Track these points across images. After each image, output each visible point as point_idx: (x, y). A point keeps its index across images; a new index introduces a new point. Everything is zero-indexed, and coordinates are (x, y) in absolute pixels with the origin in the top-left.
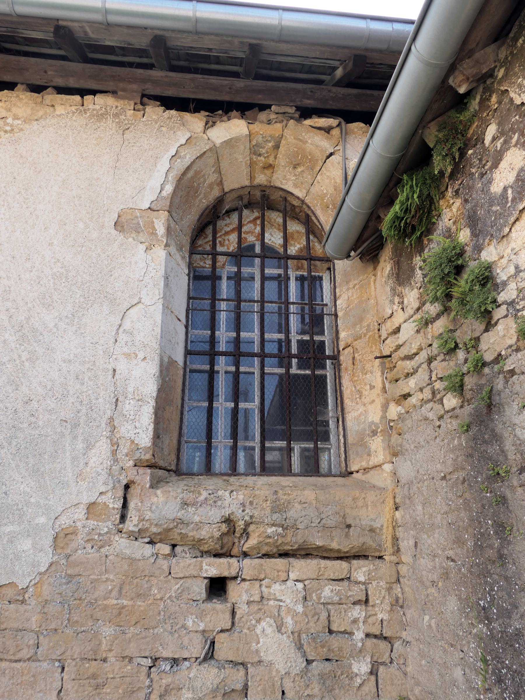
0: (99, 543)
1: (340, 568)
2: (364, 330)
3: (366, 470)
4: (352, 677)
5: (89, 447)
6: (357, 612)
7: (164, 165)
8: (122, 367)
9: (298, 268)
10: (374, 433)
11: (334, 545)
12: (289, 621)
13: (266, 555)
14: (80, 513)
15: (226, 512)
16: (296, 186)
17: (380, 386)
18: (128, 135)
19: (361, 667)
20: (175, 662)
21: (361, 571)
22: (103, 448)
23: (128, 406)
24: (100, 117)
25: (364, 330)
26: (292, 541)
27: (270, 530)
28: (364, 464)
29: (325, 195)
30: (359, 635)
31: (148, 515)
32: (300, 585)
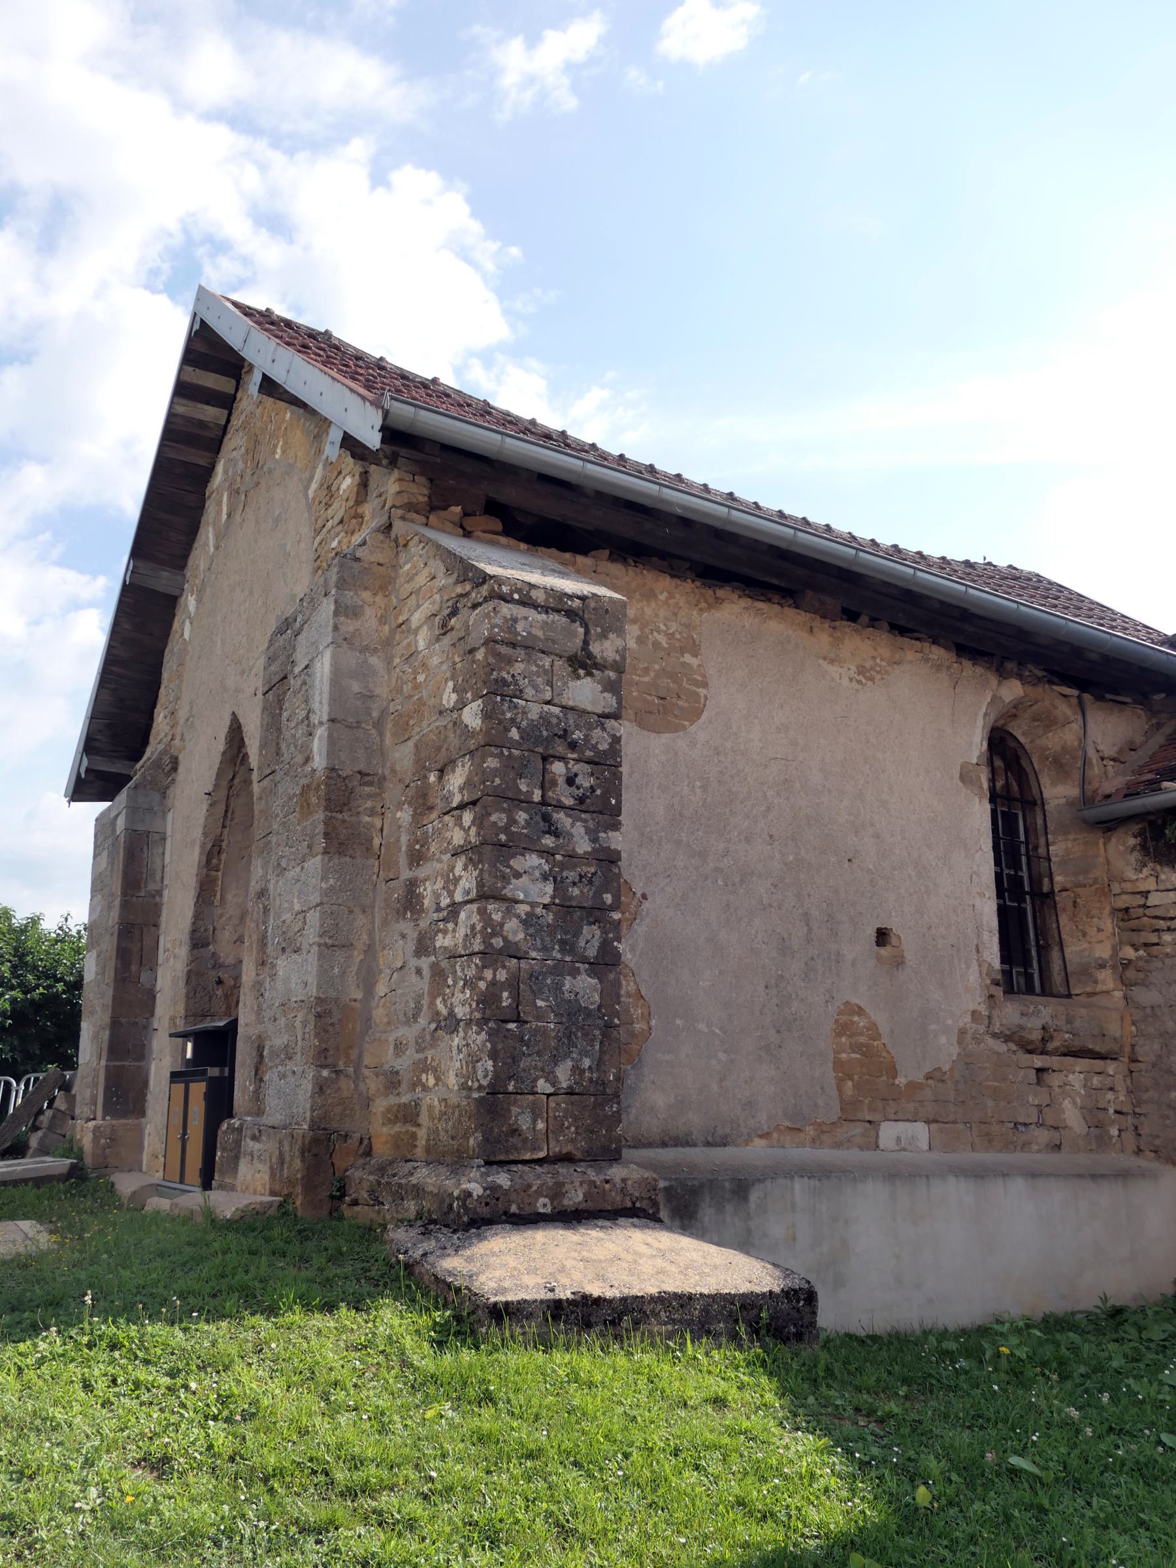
0: (977, 1040)
1: (1098, 1064)
2: (1091, 881)
3: (1090, 995)
4: (1111, 1137)
5: (968, 967)
6: (1110, 1096)
7: (980, 723)
8: (978, 903)
9: (1003, 805)
10: (1102, 966)
11: (1098, 1049)
12: (1078, 1100)
13: (1065, 1055)
14: (968, 1018)
15: (1044, 1021)
16: (1023, 734)
17: (1111, 930)
18: (958, 690)
19: (1114, 1132)
20: (1025, 1125)
21: (1111, 1067)
22: (975, 967)
23: (986, 936)
24: (938, 668)
25: (1091, 881)
26: (1077, 1044)
27: (1067, 1036)
28: (1089, 989)
29: (1049, 749)
30: (1111, 1111)
31: (1005, 1021)
32: (1082, 1076)
